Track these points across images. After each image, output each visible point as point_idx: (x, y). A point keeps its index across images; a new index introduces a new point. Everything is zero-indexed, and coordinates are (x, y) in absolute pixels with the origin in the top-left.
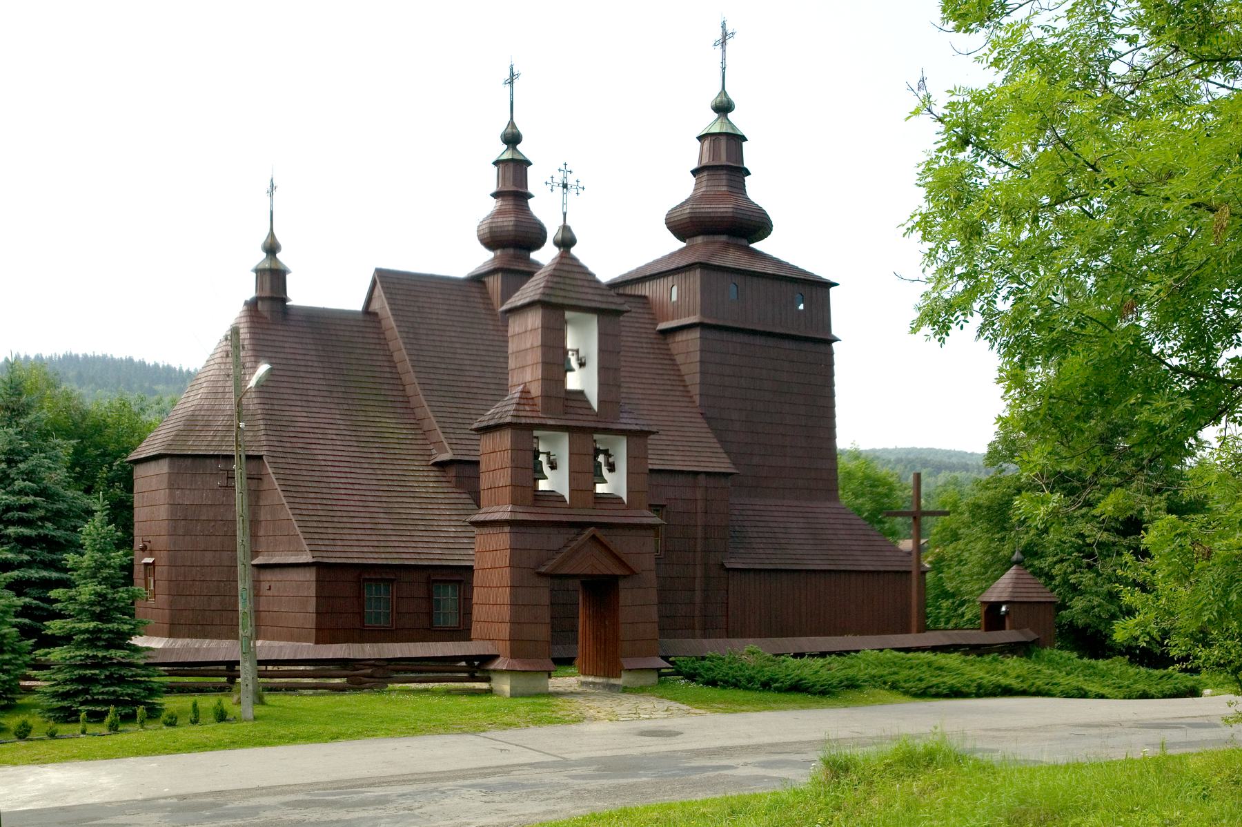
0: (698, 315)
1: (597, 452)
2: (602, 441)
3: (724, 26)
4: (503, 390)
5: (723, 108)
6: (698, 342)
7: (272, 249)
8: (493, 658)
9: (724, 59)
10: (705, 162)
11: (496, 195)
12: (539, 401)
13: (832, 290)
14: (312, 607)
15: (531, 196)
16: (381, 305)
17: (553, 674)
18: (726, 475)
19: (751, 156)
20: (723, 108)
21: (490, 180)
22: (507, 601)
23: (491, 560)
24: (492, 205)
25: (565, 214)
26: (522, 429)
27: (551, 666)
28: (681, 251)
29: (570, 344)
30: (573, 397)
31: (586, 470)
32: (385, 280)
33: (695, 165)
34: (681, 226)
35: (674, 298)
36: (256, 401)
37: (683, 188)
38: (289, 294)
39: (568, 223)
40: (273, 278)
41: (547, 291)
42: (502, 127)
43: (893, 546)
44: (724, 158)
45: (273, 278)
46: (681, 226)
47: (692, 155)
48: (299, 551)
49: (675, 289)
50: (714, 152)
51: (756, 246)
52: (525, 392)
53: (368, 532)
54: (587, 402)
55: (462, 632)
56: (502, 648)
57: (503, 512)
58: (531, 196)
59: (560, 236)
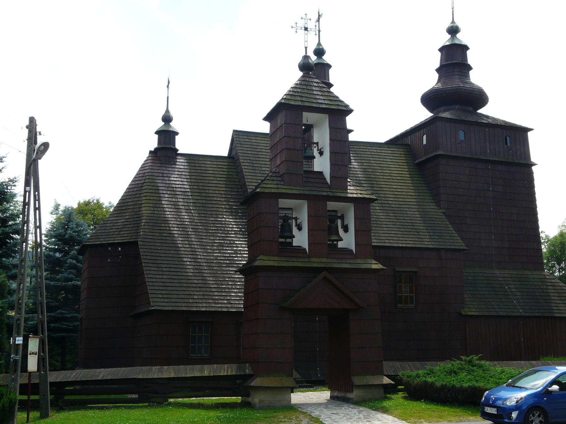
5: (453, 31)
7: (167, 119)
13: (530, 134)
17: (294, 390)
18: (464, 250)
19: (471, 58)
20: (453, 31)
25: (306, 48)
27: (294, 385)
34: (429, 100)
35: (425, 142)
37: (430, 80)
38: (177, 146)
40: (167, 136)
41: (289, 97)
44: (454, 59)
45: (167, 136)
46: (429, 100)
47: (436, 60)
51: (479, 111)
54: (325, 179)
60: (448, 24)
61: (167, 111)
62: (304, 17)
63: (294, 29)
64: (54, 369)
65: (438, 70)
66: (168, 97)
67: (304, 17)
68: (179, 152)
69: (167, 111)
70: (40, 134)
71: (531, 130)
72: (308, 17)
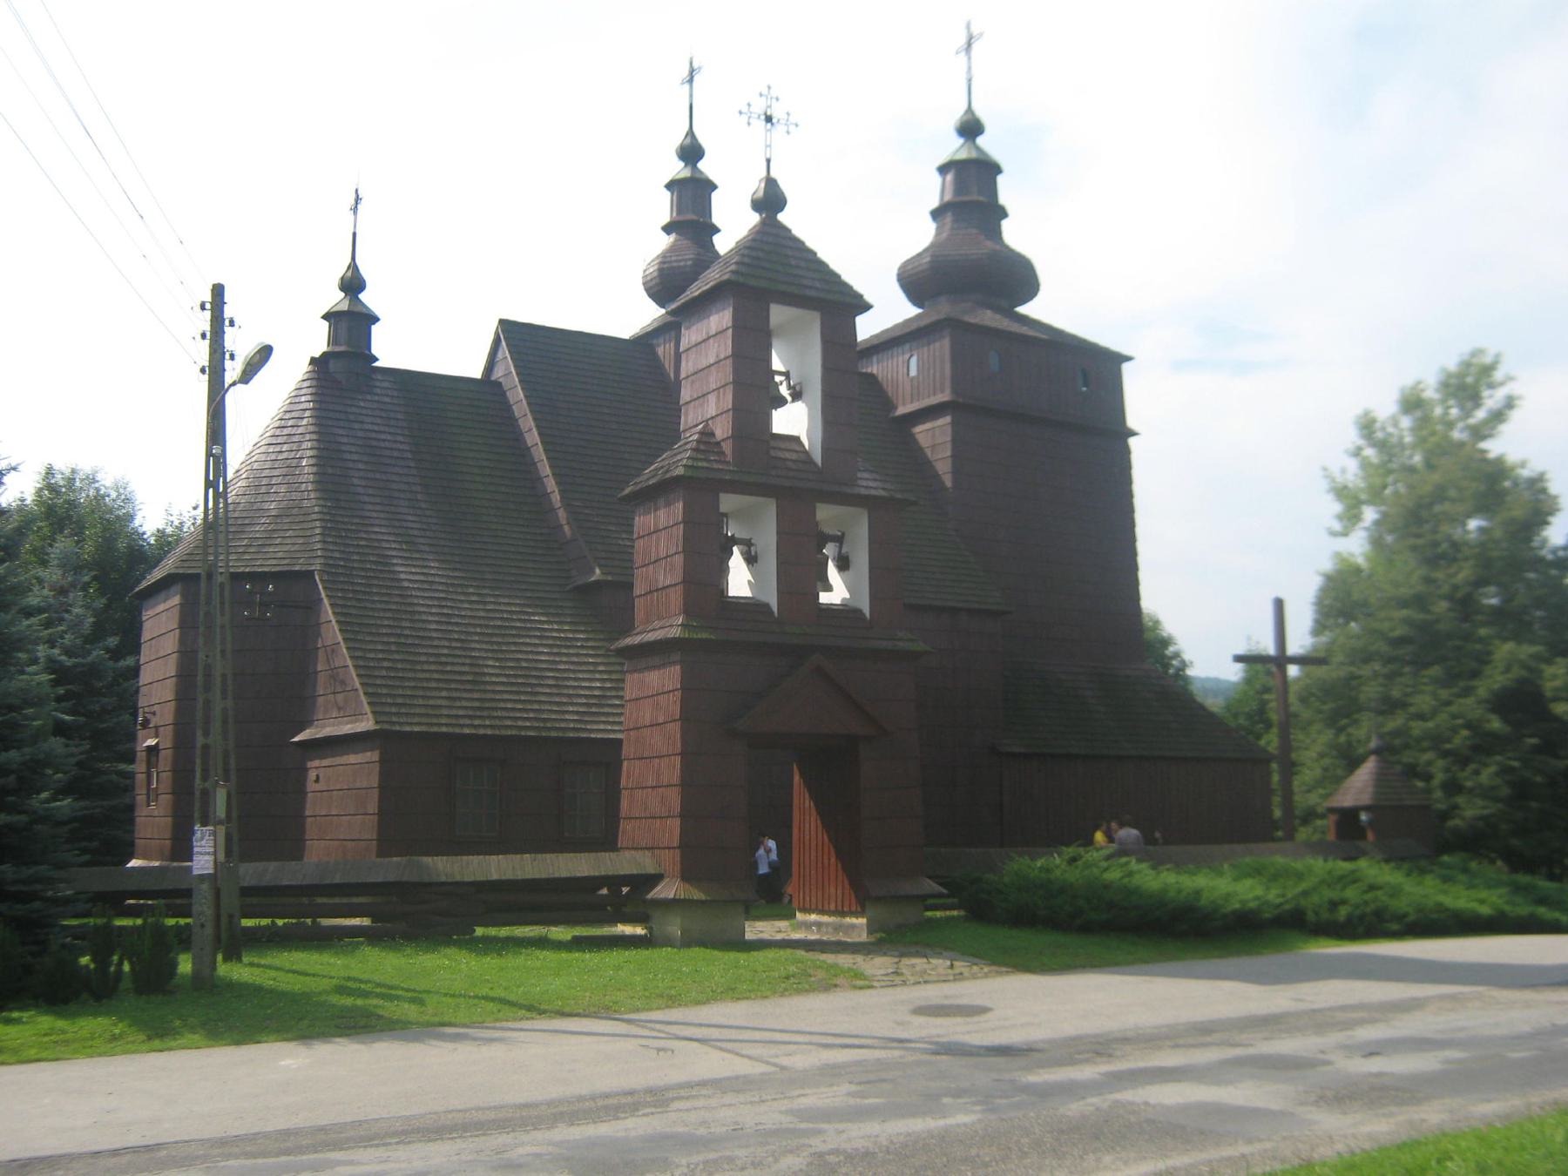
0: (948, 391)
1: (824, 539)
2: (826, 514)
3: (968, 26)
4: (670, 433)
6: (949, 430)
7: (353, 284)
8: (653, 880)
9: (970, 68)
10: (948, 197)
11: (667, 229)
12: (727, 448)
14: (373, 807)
15: (717, 230)
16: (507, 371)
19: (1007, 191)
21: (662, 208)
22: (676, 779)
23: (648, 714)
24: (665, 241)
25: (768, 161)
26: (699, 490)
28: (918, 317)
29: (777, 364)
30: (783, 445)
31: (799, 575)
32: (516, 337)
33: (935, 203)
35: (913, 372)
36: (312, 495)
39: (773, 174)
40: (352, 324)
41: (743, 269)
42: (678, 137)
43: (1097, 828)
47: (932, 190)
48: (357, 715)
49: (914, 361)
50: (960, 186)
51: (1022, 310)
52: (707, 434)
53: (468, 687)
55: (607, 841)
56: (670, 861)
57: (672, 628)
58: (717, 230)
59: (761, 194)
60: (957, 113)
61: (353, 266)
62: (765, 92)
63: (744, 118)
64: (245, 857)
65: (936, 214)
66: (354, 235)
67: (765, 92)
68: (377, 364)
69: (353, 266)
70: (232, 323)
71: (1129, 359)
72: (774, 93)
